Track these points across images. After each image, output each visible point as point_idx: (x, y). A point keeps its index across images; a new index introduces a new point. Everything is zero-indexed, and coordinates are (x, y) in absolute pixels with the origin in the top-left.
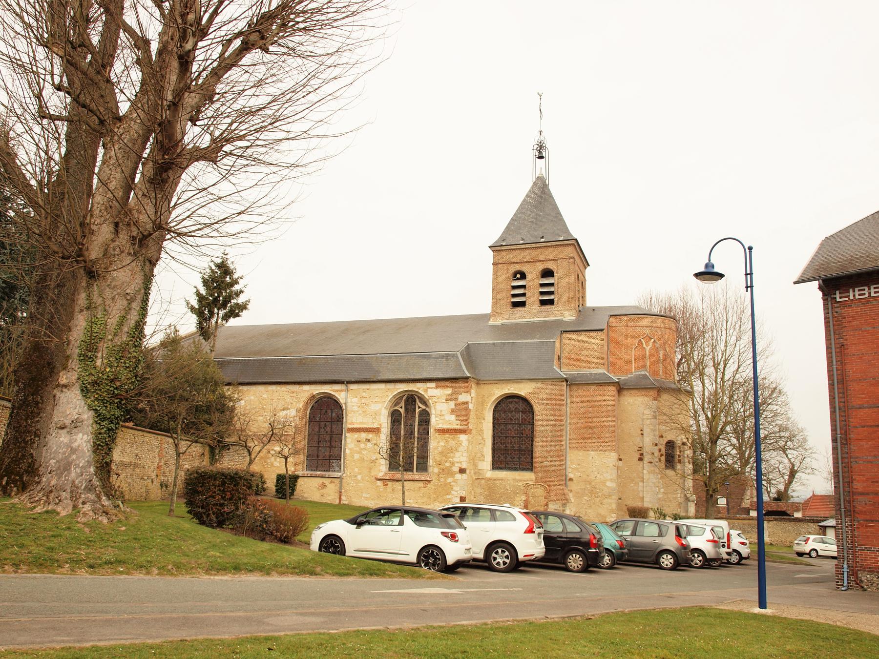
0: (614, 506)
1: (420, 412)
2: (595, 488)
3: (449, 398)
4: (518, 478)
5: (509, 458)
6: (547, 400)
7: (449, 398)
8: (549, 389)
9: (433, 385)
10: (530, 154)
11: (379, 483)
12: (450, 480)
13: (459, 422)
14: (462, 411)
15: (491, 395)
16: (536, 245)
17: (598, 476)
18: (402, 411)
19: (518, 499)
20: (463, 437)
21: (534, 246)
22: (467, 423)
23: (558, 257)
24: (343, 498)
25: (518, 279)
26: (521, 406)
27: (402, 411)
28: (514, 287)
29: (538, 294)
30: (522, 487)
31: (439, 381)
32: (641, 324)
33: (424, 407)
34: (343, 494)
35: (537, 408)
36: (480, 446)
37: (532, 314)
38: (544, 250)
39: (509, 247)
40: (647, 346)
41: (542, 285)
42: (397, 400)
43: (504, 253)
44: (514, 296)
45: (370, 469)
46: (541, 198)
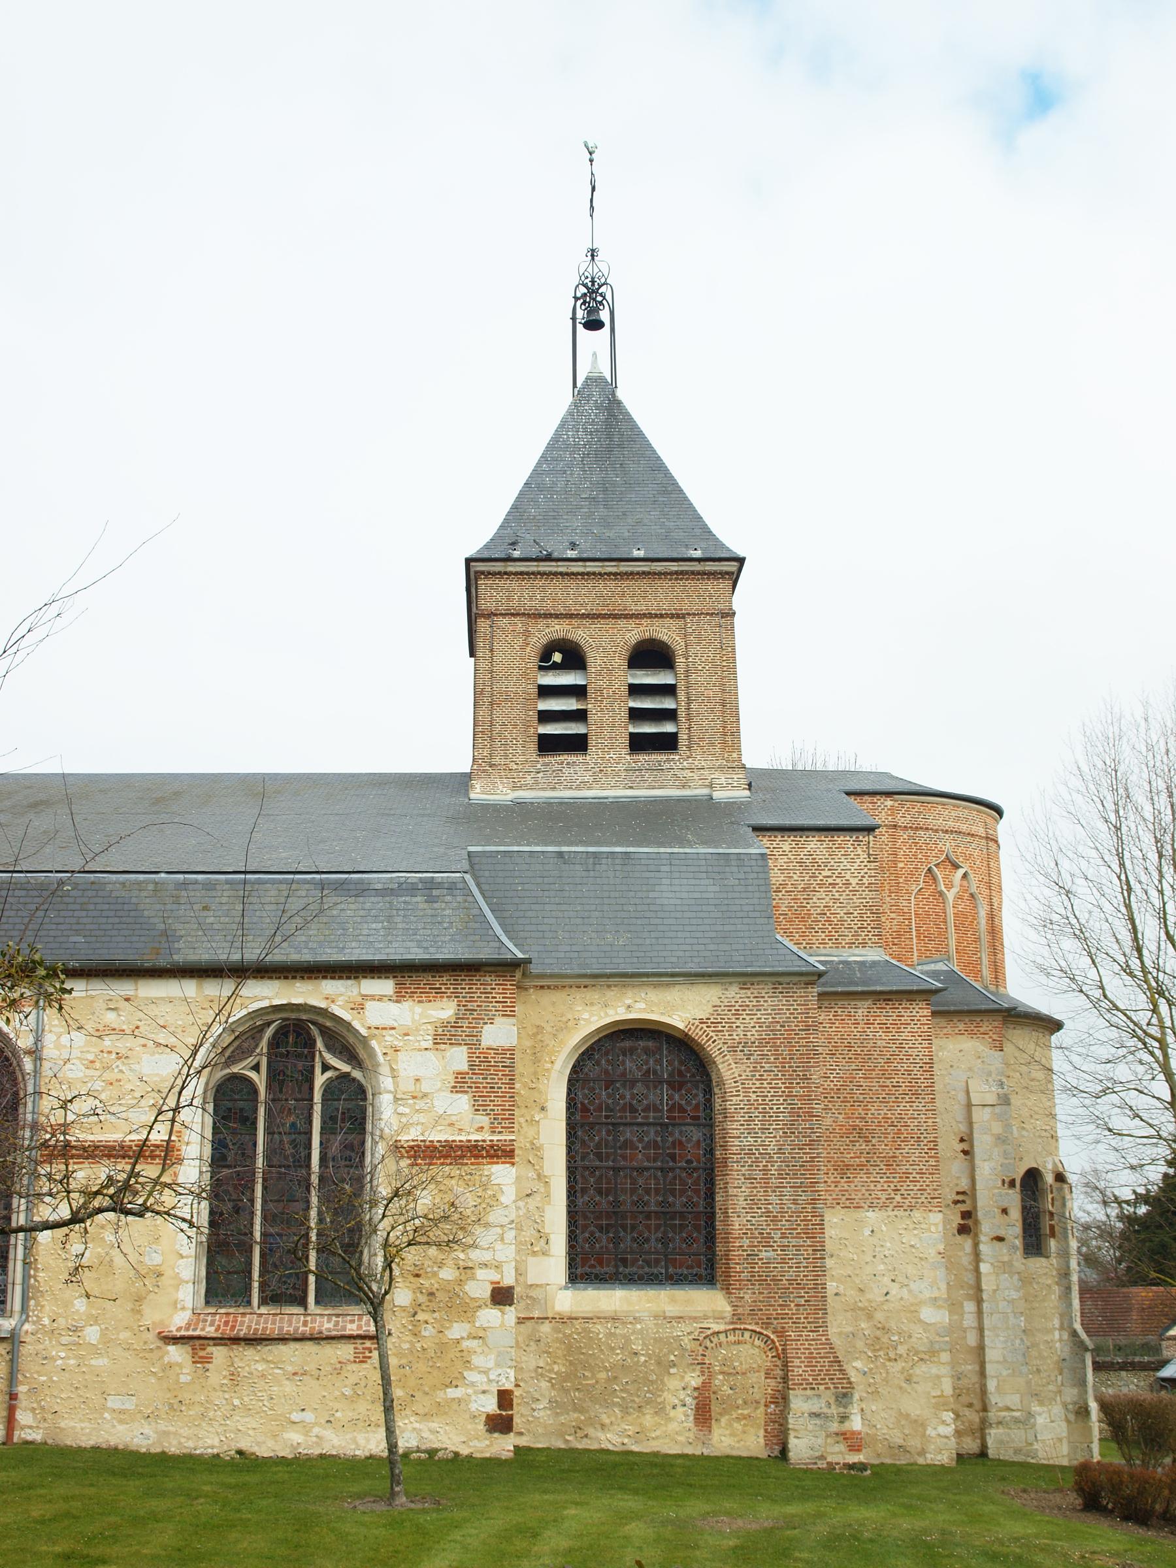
0: (947, 1387)
1: (330, 1090)
2: (885, 1330)
3: (445, 1036)
4: (672, 1310)
5: (627, 1242)
6: (762, 1043)
7: (445, 1036)
8: (761, 1011)
9: (386, 986)
10: (562, 305)
11: (175, 1353)
12: (457, 1330)
13: (484, 1121)
14: (491, 1079)
15: (564, 1027)
16: (617, 567)
17: (894, 1289)
18: (260, 1080)
19: (673, 1383)
20: (501, 1174)
21: (610, 567)
22: (504, 1119)
23: (686, 607)
24: (23, 1417)
25: (555, 667)
26: (666, 1063)
27: (260, 1080)
28: (546, 691)
29: (625, 714)
30: (686, 1342)
31: (408, 973)
32: (932, 822)
33: (345, 1068)
34: (23, 1402)
35: (730, 1070)
36: (533, 1203)
37: (606, 774)
38: (643, 583)
39: (532, 567)
40: (950, 886)
41: (636, 690)
42: (243, 1040)
43: (514, 584)
44: (546, 717)
45: (139, 1299)
46: (610, 437)
